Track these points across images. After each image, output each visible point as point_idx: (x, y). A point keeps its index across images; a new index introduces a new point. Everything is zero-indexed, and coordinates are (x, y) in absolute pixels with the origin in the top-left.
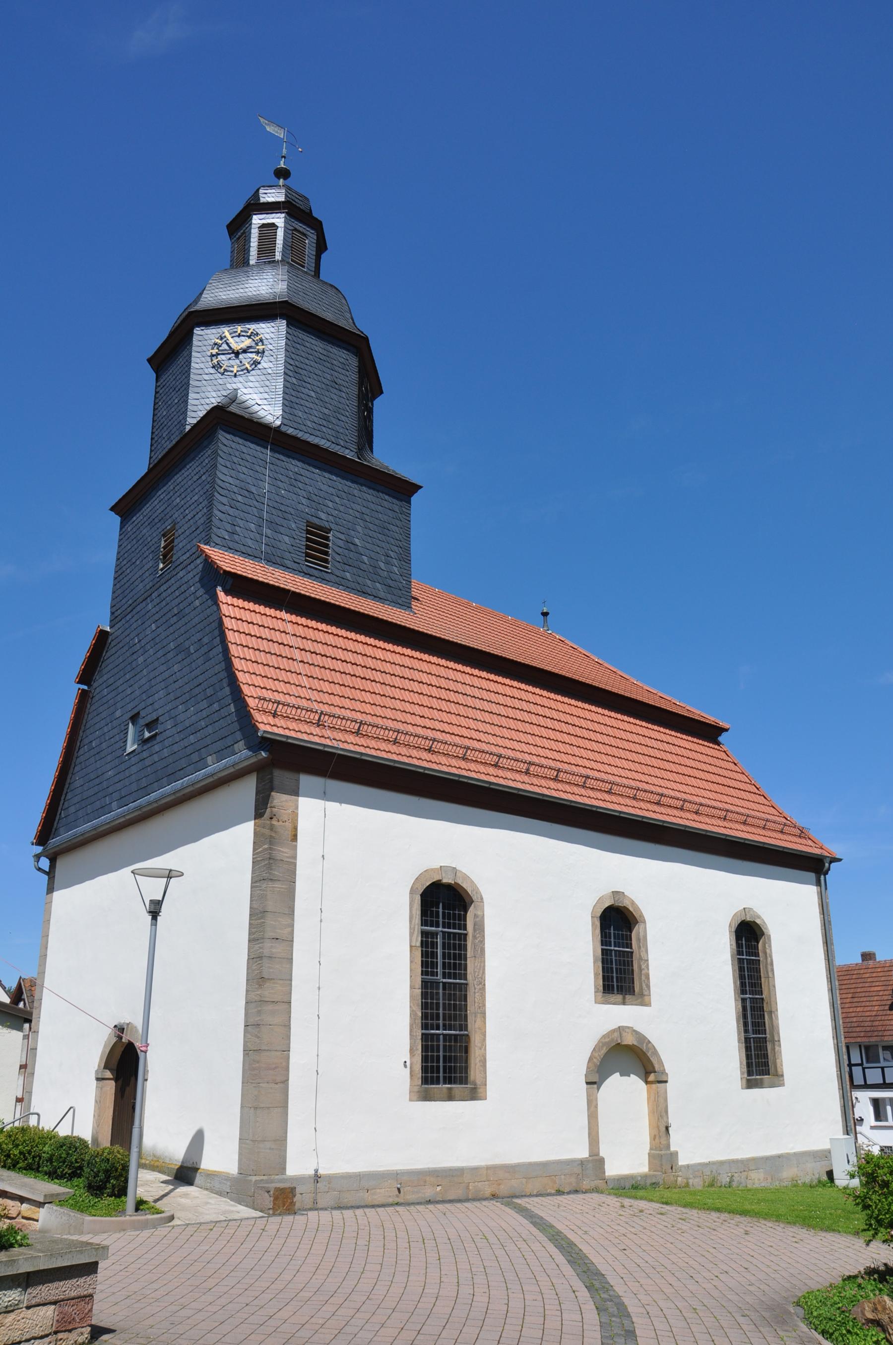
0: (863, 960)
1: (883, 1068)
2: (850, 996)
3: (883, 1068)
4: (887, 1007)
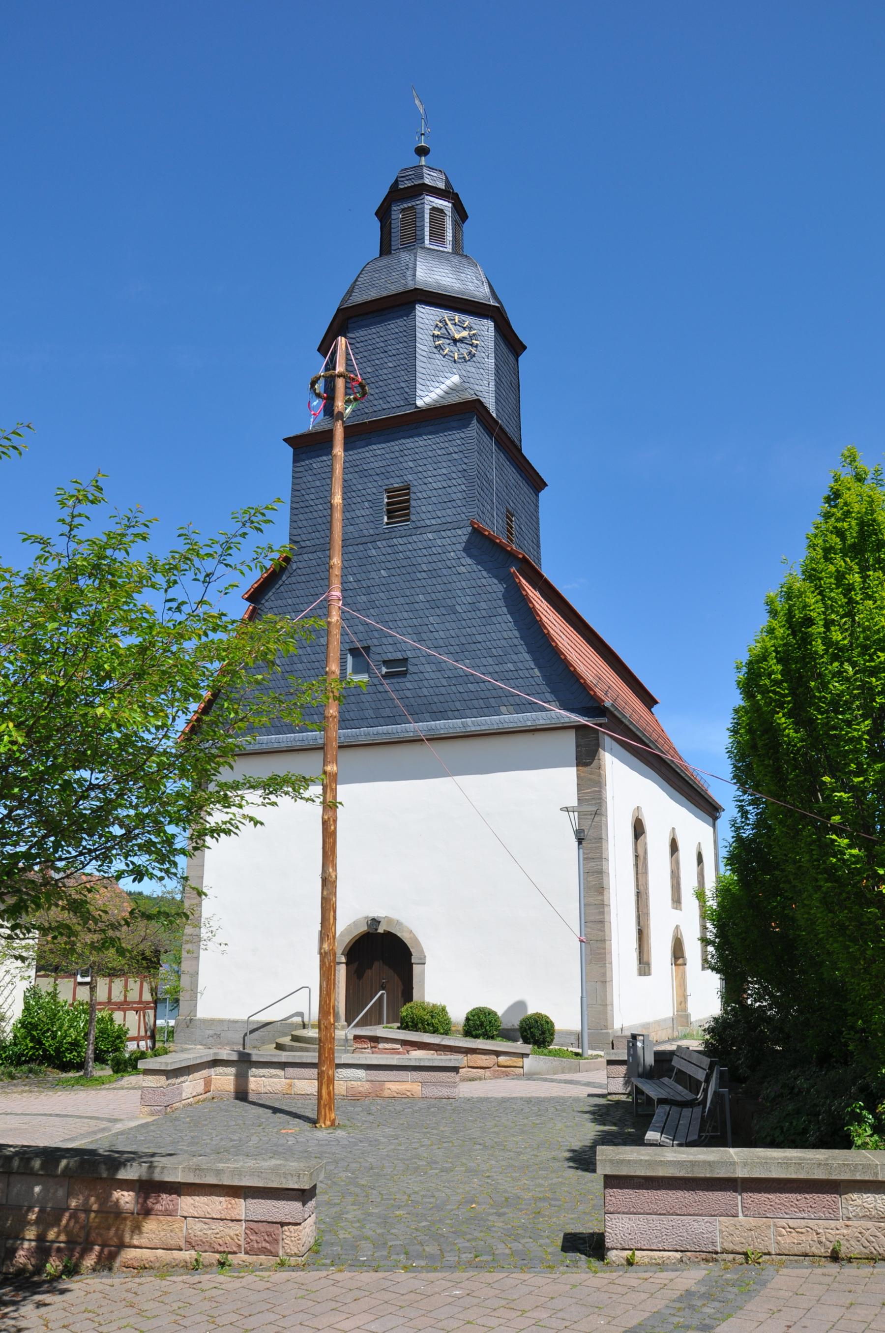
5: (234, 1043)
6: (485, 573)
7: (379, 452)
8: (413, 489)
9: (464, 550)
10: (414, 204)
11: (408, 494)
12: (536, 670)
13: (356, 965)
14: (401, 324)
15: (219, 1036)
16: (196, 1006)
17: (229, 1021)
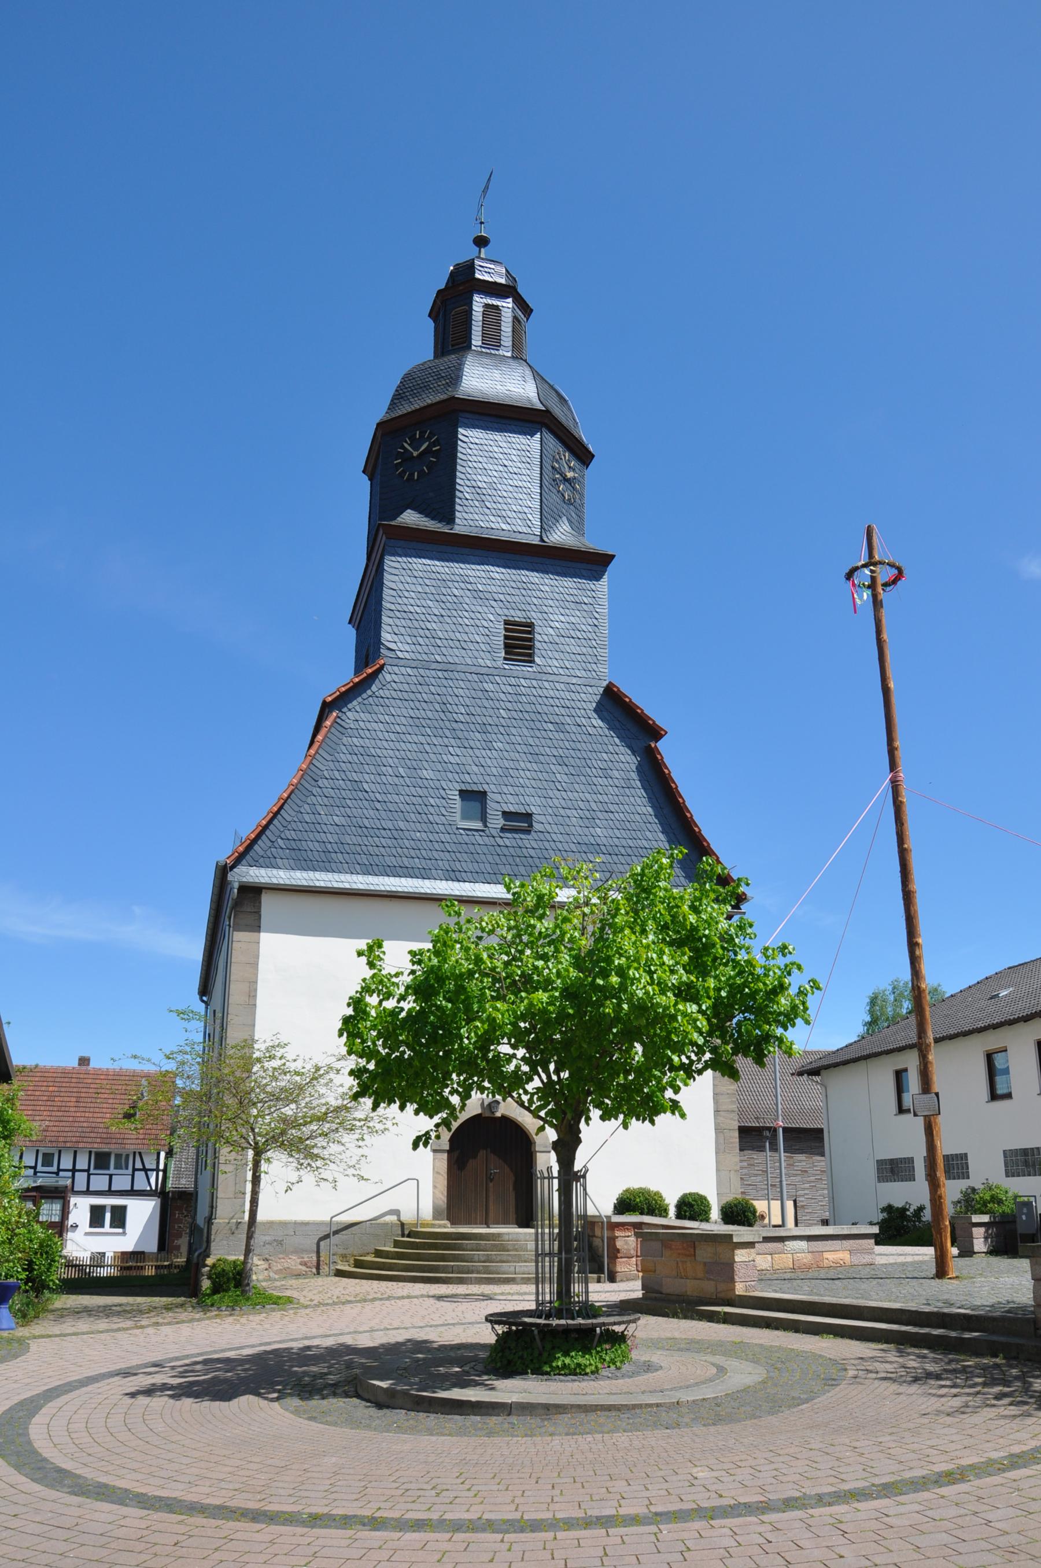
0: (80, 1064)
1: (111, 1176)
2: (74, 1099)
3: (111, 1176)
4: (120, 1116)
5: (303, 1251)
6: (617, 740)
7: (497, 576)
8: (537, 629)
9: (595, 710)
10: (499, 303)
11: (529, 632)
13: (456, 1154)
14: (524, 441)
15: (280, 1243)
17: (295, 1223)
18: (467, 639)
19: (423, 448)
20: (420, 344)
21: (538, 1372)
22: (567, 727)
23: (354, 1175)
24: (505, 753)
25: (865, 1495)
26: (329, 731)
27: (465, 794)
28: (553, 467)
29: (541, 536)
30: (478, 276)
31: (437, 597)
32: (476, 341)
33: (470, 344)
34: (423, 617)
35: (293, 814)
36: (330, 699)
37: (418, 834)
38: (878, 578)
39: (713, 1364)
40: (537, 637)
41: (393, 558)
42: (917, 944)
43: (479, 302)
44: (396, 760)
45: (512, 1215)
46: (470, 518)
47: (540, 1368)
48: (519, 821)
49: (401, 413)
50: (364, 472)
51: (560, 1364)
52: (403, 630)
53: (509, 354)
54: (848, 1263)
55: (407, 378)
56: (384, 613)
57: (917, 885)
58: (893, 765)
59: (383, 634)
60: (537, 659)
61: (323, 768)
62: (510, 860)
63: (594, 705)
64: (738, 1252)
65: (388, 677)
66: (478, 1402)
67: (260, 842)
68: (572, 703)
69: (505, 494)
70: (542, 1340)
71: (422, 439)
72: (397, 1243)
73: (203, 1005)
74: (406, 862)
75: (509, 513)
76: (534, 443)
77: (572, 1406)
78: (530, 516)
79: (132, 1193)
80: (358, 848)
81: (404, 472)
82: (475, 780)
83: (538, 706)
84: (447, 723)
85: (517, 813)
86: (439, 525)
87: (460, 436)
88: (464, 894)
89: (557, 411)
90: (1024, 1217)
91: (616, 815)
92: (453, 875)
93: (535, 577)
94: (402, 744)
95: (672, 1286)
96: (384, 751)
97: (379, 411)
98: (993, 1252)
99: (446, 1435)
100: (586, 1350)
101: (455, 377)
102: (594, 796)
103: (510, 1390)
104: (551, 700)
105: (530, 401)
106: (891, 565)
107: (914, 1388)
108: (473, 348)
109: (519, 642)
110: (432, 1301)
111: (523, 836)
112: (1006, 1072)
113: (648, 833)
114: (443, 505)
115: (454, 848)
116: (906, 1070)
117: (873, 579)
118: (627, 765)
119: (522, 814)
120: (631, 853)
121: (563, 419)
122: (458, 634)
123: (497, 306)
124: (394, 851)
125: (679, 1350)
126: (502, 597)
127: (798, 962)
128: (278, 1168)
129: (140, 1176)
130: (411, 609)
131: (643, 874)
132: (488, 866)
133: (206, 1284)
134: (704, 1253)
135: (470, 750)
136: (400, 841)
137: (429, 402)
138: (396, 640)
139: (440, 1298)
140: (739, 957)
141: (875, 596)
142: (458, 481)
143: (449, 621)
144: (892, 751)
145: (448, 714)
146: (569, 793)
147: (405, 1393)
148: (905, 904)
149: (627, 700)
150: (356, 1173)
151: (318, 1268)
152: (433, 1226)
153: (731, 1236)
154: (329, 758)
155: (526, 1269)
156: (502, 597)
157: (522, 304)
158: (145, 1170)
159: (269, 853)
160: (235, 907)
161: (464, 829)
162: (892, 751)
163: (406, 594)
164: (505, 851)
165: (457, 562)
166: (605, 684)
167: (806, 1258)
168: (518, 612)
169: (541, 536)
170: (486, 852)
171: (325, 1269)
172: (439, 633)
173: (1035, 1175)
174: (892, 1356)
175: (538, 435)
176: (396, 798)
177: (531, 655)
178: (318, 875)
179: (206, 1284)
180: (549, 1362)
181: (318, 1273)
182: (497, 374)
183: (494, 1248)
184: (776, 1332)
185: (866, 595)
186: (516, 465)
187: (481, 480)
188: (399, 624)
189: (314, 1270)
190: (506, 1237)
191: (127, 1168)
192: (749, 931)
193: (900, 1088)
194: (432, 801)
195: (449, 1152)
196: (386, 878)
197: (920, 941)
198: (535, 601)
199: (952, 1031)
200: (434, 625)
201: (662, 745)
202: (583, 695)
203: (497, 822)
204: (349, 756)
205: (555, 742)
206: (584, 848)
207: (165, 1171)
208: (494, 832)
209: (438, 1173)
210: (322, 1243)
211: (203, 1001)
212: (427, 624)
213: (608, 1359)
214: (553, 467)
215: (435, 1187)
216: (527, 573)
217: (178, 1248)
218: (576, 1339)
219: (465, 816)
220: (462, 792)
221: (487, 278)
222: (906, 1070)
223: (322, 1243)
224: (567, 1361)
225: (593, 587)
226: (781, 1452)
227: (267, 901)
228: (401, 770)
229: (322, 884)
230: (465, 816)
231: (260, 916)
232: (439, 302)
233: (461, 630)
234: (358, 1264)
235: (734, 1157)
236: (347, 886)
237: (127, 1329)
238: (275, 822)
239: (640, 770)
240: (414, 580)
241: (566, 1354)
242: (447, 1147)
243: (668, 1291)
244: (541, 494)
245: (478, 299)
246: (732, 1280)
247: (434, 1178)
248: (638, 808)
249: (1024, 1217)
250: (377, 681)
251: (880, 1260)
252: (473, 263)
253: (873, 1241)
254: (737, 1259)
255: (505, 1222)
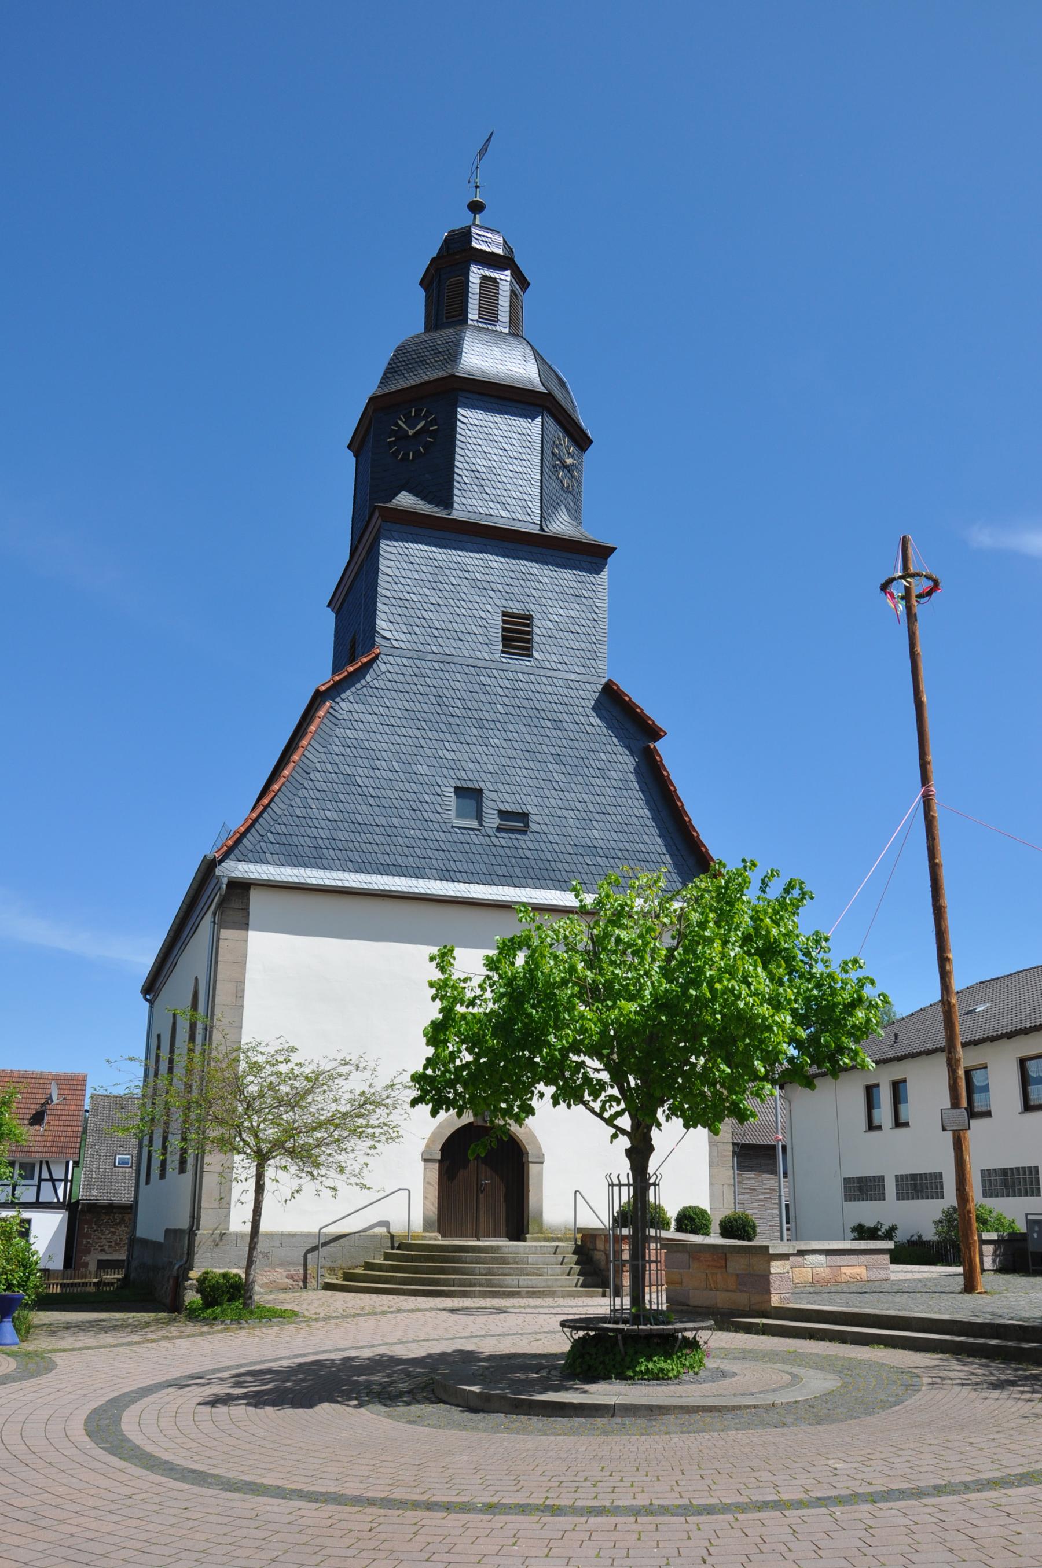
5: (290, 1264)
6: (615, 740)
8: (536, 622)
9: (594, 709)
10: (497, 276)
11: (527, 625)
12: (668, 856)
16: (228, 1215)
17: (282, 1234)
18: (464, 630)
19: (419, 427)
20: (408, 316)
21: (622, 1377)
22: (565, 724)
23: (357, 1184)
24: (502, 750)
25: (1007, 1483)
26: (322, 722)
27: (461, 792)
28: (553, 454)
29: (541, 525)
30: (475, 244)
31: (434, 584)
32: (473, 315)
33: (467, 318)
34: (419, 605)
35: (284, 807)
36: (323, 688)
37: (412, 832)
38: (913, 590)
39: (787, 1373)
40: (535, 629)
41: (389, 543)
42: (948, 959)
43: (476, 274)
44: (390, 754)
45: (503, 1229)
46: (469, 504)
47: (623, 1372)
48: (516, 821)
49: (395, 388)
50: (349, 447)
51: (643, 1368)
52: (398, 619)
53: (506, 331)
54: (864, 1278)
55: (400, 351)
56: (380, 599)
57: (948, 899)
58: (925, 780)
59: (378, 622)
60: (535, 654)
61: (315, 760)
62: (506, 860)
63: (593, 702)
64: (773, 1264)
65: (383, 668)
66: (580, 1404)
67: (249, 836)
68: (570, 699)
69: (505, 480)
70: (624, 1344)
71: (418, 418)
72: (387, 1256)
73: (147, 1004)
74: (400, 860)
75: (508, 499)
76: (535, 427)
77: (675, 1407)
78: (530, 504)
79: (38, 1205)
80: (351, 845)
81: (398, 451)
82: (470, 778)
83: (536, 702)
84: (443, 717)
85: (513, 812)
86: (436, 509)
87: (459, 417)
88: (459, 895)
89: (558, 394)
90: (1035, 1235)
91: (613, 817)
92: (448, 875)
93: (534, 568)
94: (397, 737)
95: (698, 1298)
96: (378, 744)
97: (369, 385)
98: (1002, 1270)
99: (560, 1435)
100: (668, 1355)
101: (454, 354)
102: (591, 797)
103: (602, 1393)
104: (549, 696)
105: (531, 382)
106: (928, 577)
107: (996, 1394)
108: (470, 322)
109: (517, 635)
110: (445, 1314)
111: (519, 837)
112: (986, 1089)
113: (645, 837)
114: (440, 485)
115: (449, 846)
116: (877, 1085)
117: (907, 589)
118: (625, 766)
119: (519, 813)
120: (627, 857)
121: (563, 403)
122: (455, 625)
123: (495, 279)
124: (387, 848)
125: (735, 1358)
126: (500, 587)
127: (871, 977)
128: (281, 1177)
129: (46, 1186)
130: (407, 596)
131: (727, 888)
132: (483, 866)
133: (192, 1297)
134: (737, 1265)
135: (466, 746)
136: (393, 838)
137: (427, 378)
138: (392, 628)
139: (452, 1311)
140: (814, 971)
141: (909, 608)
142: (457, 463)
143: (446, 611)
144: (924, 765)
145: (444, 707)
146: (566, 793)
147: (502, 1397)
148: (935, 919)
149: (627, 699)
150: (359, 1181)
151: (305, 1281)
152: (424, 1238)
153: (767, 1247)
154: (321, 749)
155: (530, 1283)
156: (500, 587)
157: (521, 280)
158: (52, 1180)
159: (258, 848)
160: (216, 901)
161: (459, 828)
162: (924, 765)
163: (402, 580)
164: (501, 851)
165: (455, 549)
166: (604, 681)
167: (824, 1272)
168: (516, 603)
169: (541, 525)
170: (482, 852)
171: (312, 1282)
172: (436, 623)
173: (1014, 1196)
174: (954, 1365)
175: (539, 419)
176: (390, 793)
177: (528, 649)
178: (309, 872)
179: (192, 1297)
180: (632, 1367)
181: (305, 1287)
182: (497, 351)
183: (495, 1261)
184: (822, 1343)
185: (901, 607)
186: (515, 447)
187: (480, 464)
188: (394, 611)
189: (301, 1284)
190: (506, 1250)
191: (32, 1178)
192: (824, 944)
193: (871, 1103)
194: (426, 797)
195: (440, 1161)
196: (379, 876)
197: (950, 956)
198: (534, 592)
199: (929, 1047)
200: (430, 614)
201: (660, 746)
202: (581, 692)
203: (492, 820)
204: (341, 748)
205: (552, 739)
206: (581, 850)
207: (71, 1181)
208: (490, 832)
209: (429, 1183)
210: (309, 1256)
211: (147, 1000)
212: (423, 612)
213: (687, 1364)
214: (553, 454)
215: (425, 1198)
216: (526, 563)
217: (86, 1265)
218: (658, 1344)
219: (460, 815)
220: (457, 789)
221: (484, 247)
222: (877, 1085)
223: (309, 1256)
224: (650, 1365)
225: (593, 579)
226: (903, 1447)
227: (256, 897)
228: (395, 764)
229: (314, 881)
230: (460, 815)
231: (248, 913)
232: (432, 271)
233: (458, 621)
234: (347, 1277)
235: (728, 1171)
236: (340, 884)
237: (136, 1343)
238: (265, 815)
239: (637, 771)
240: (411, 566)
241: (649, 1359)
242: (439, 1157)
243: (696, 1304)
244: (541, 481)
245: (475, 270)
246: (768, 1292)
247: (425, 1188)
248: (635, 810)
249: (1035, 1235)
250: (371, 671)
251: (893, 1277)
252: (470, 231)
253: (888, 1257)
254: (773, 1270)
255: (496, 1235)
